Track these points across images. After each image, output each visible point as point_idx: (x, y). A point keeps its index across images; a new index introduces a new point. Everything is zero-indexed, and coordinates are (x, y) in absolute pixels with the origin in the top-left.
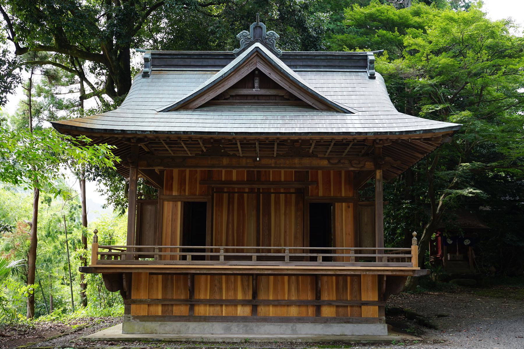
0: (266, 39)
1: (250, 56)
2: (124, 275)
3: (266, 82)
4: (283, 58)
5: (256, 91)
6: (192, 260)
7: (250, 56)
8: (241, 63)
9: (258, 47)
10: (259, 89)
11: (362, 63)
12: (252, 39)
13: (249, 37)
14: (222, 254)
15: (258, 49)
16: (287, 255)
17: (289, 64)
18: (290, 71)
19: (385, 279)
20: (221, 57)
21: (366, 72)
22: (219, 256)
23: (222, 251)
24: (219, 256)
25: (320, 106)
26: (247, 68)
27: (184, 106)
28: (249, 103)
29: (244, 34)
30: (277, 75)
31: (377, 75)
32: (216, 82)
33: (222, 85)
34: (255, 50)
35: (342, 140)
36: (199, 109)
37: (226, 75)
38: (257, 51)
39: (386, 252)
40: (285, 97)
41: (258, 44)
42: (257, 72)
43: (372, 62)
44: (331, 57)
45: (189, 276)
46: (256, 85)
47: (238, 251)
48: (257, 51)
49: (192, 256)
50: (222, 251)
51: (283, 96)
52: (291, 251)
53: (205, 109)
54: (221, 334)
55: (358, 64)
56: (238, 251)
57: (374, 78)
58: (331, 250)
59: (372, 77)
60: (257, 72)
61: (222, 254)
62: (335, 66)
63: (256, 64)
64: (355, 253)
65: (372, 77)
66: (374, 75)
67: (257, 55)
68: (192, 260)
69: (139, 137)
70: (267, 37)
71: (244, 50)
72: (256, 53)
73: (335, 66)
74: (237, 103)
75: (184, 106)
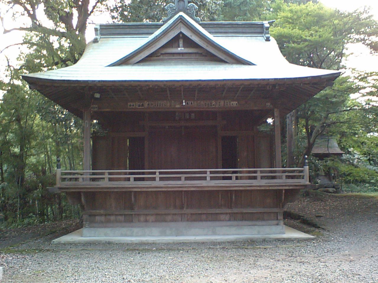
0: (188, 9)
1: (176, 23)
2: (82, 194)
3: (188, 42)
4: (204, 26)
5: (181, 49)
6: (185, 180)
7: (176, 23)
8: (169, 28)
9: (182, 16)
10: (183, 49)
11: (259, 30)
12: (177, 9)
13: (174, 8)
14: (208, 175)
15: (182, 18)
16: (259, 175)
17: (209, 31)
18: (210, 36)
19: (284, 192)
20: (211, 26)
21: (263, 36)
22: (206, 177)
23: (157, 173)
24: (206, 177)
25: (234, 61)
26: (173, 32)
27: (125, 62)
28: (176, 59)
29: (171, 6)
30: (197, 37)
31: (271, 38)
32: (150, 43)
33: (154, 45)
34: (179, 18)
35: (181, 86)
36: (138, 64)
37: (157, 37)
38: (181, 19)
39: (284, 172)
40: (203, 54)
41: (181, 13)
42: (181, 35)
43: (267, 28)
44: (236, 26)
45: (133, 194)
46: (181, 45)
47: (271, 172)
48: (181, 19)
49: (135, 178)
50: (157, 173)
51: (201, 54)
52: (211, 172)
53: (140, 64)
54: (255, 234)
55: (257, 31)
56: (271, 172)
57: (269, 40)
58: (243, 171)
59: (268, 40)
60: (181, 35)
61: (208, 175)
62: (240, 32)
63: (180, 28)
64: (109, 175)
65: (268, 40)
66: (269, 38)
67: (181, 22)
68: (185, 180)
69: (91, 85)
70: (188, 8)
71: (171, 18)
72: (180, 21)
73: (240, 32)
74: (166, 59)
75: (125, 62)
